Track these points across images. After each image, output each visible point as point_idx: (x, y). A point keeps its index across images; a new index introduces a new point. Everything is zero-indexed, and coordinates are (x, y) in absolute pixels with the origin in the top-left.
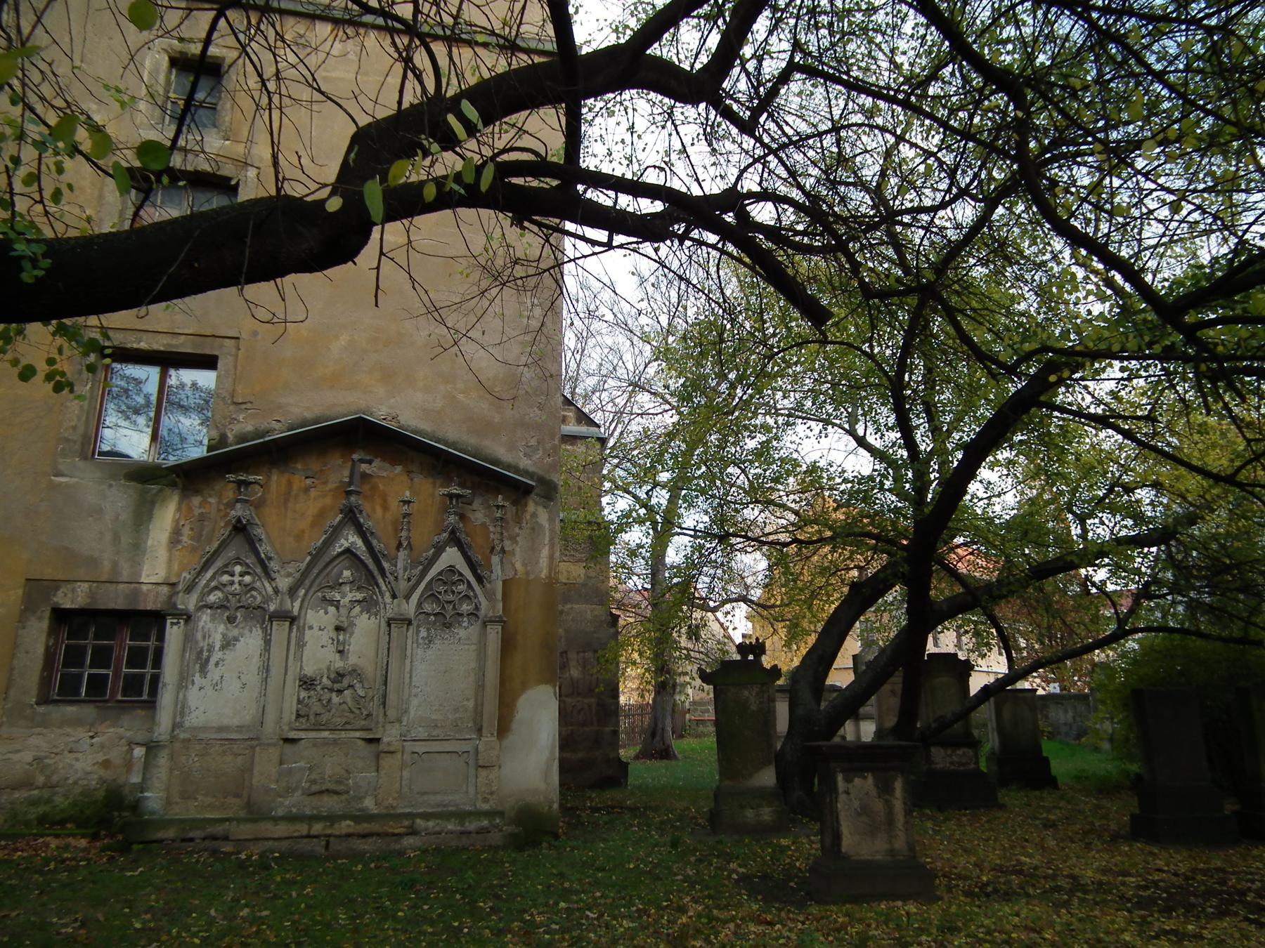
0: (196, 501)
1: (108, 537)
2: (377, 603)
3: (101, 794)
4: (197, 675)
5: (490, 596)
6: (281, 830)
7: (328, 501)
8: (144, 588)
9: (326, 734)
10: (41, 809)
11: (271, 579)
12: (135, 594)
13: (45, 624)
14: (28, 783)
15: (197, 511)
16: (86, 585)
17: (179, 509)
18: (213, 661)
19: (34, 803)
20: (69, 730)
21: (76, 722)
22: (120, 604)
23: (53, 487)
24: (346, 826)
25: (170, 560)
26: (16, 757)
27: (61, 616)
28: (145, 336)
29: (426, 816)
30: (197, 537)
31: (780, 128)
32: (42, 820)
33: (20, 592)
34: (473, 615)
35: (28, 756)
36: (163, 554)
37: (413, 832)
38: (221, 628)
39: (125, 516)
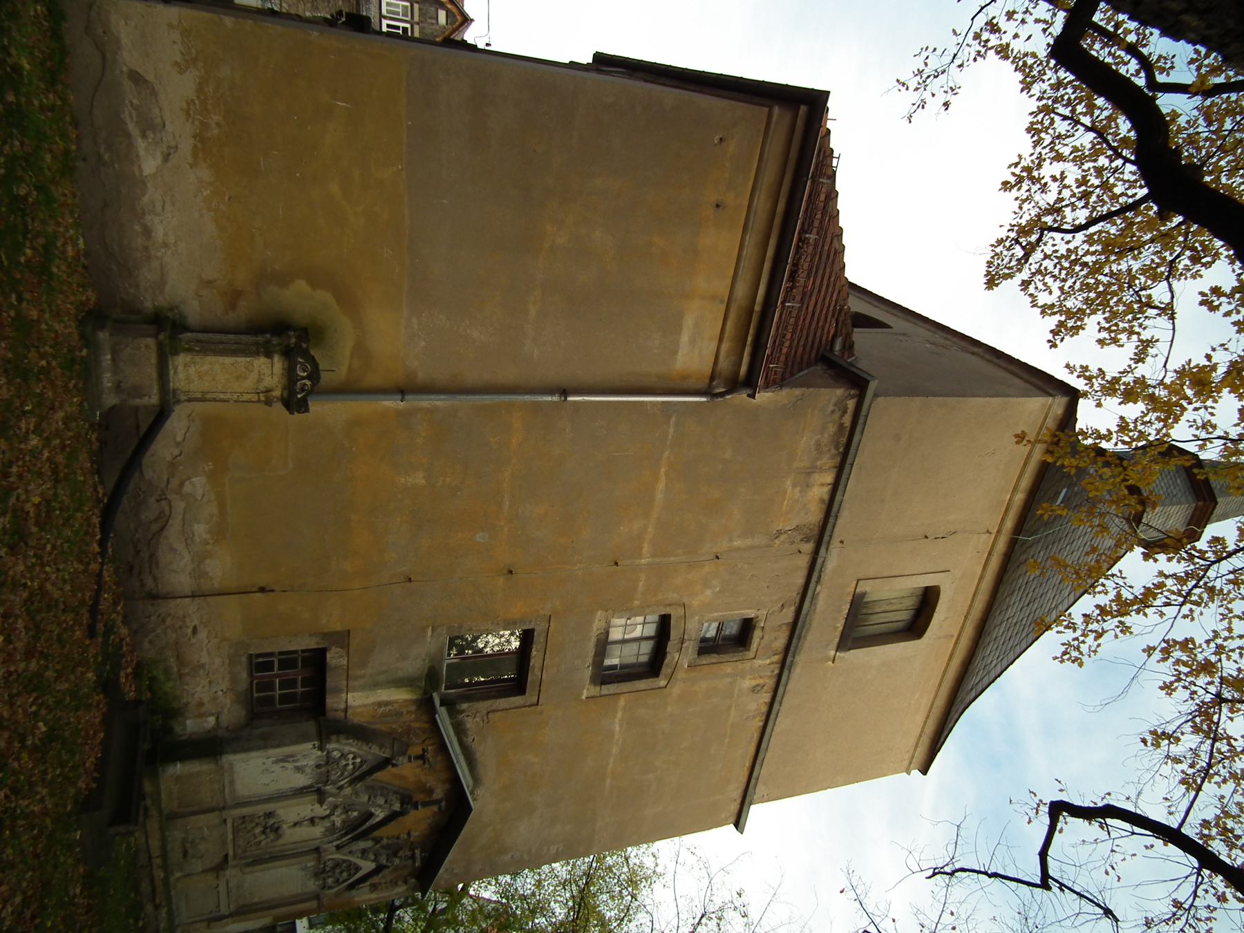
0: (413, 708)
1: (384, 668)
2: (332, 834)
3: (175, 705)
4: (140, 140)
5: (338, 895)
6: (155, 843)
7: (412, 779)
8: (344, 695)
9: (230, 836)
10: (162, 677)
11: (352, 782)
12: (338, 691)
13: (313, 646)
14: (181, 661)
15: (404, 710)
16: (345, 662)
17: (405, 701)
18: (286, 764)
19: (167, 671)
20: (227, 678)
21: (234, 680)
22: (330, 683)
23: (424, 629)
24: (159, 874)
25: (365, 706)
26: (204, 653)
27: (321, 654)
28: (541, 654)
29: (170, 914)
30: (384, 715)
31: (834, 337)
32: (153, 679)
33: (339, 628)
34: (324, 887)
35: (205, 659)
36: (371, 700)
37: (157, 907)
38: (311, 763)
39: (400, 674)
